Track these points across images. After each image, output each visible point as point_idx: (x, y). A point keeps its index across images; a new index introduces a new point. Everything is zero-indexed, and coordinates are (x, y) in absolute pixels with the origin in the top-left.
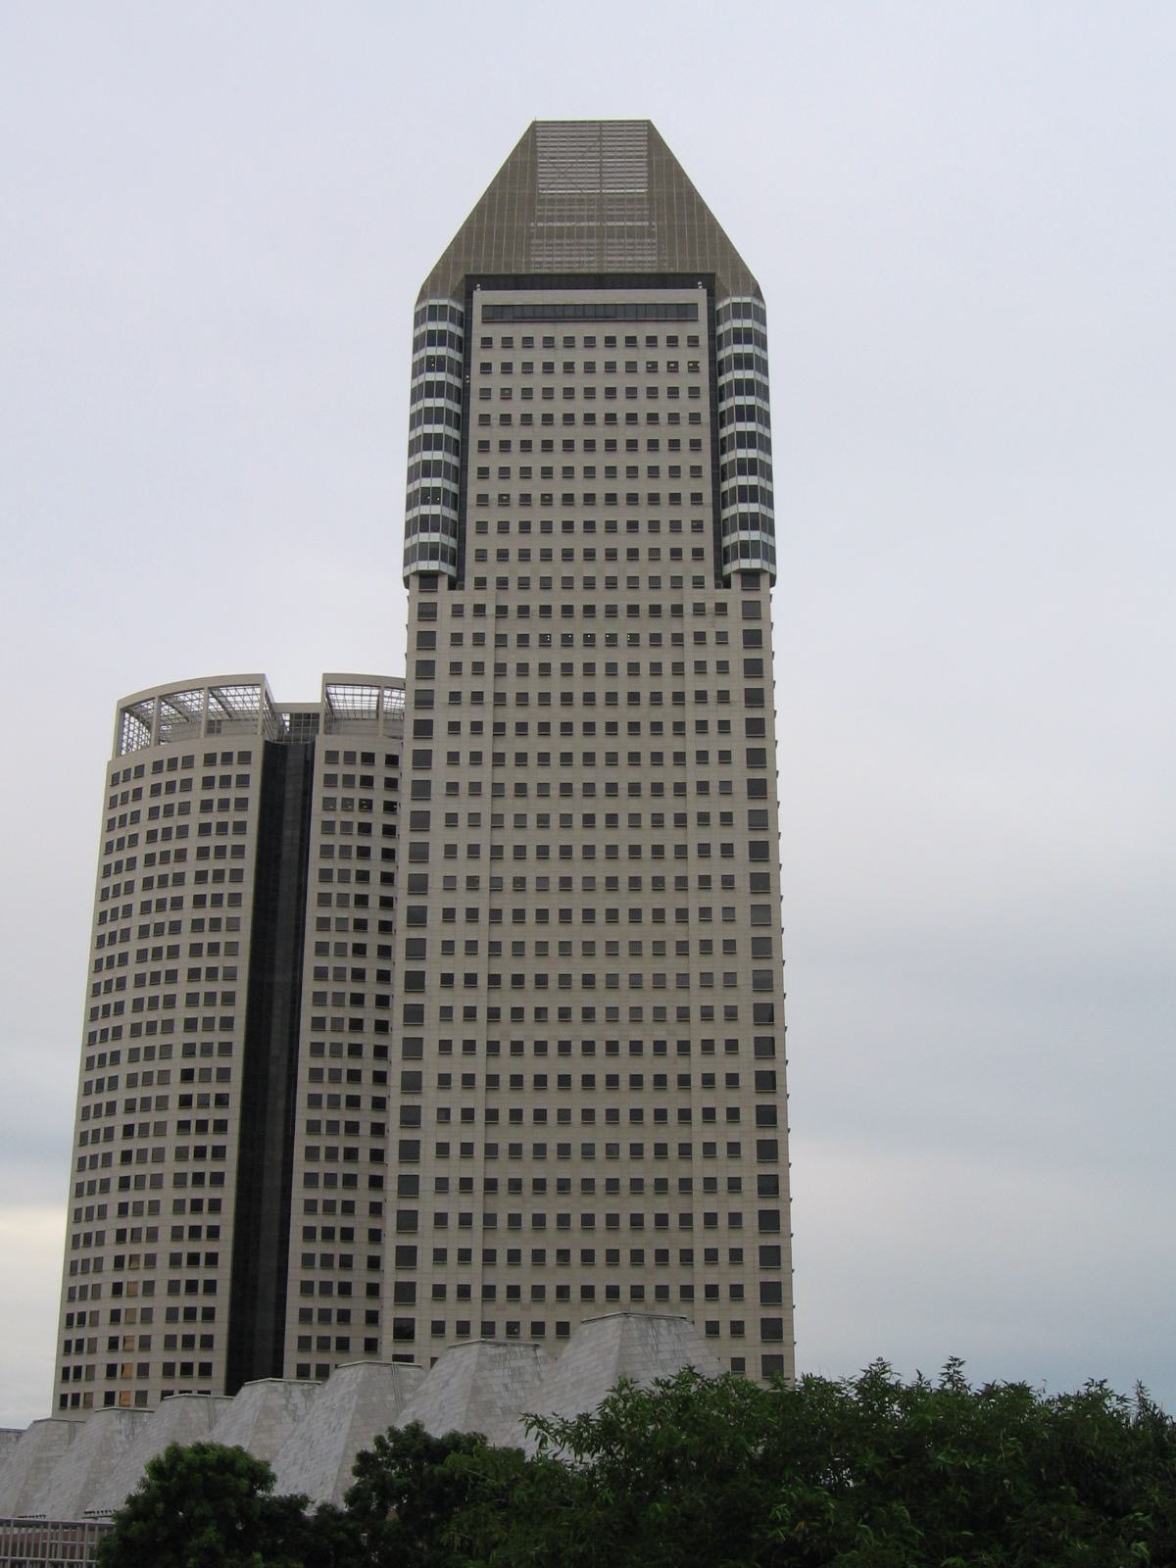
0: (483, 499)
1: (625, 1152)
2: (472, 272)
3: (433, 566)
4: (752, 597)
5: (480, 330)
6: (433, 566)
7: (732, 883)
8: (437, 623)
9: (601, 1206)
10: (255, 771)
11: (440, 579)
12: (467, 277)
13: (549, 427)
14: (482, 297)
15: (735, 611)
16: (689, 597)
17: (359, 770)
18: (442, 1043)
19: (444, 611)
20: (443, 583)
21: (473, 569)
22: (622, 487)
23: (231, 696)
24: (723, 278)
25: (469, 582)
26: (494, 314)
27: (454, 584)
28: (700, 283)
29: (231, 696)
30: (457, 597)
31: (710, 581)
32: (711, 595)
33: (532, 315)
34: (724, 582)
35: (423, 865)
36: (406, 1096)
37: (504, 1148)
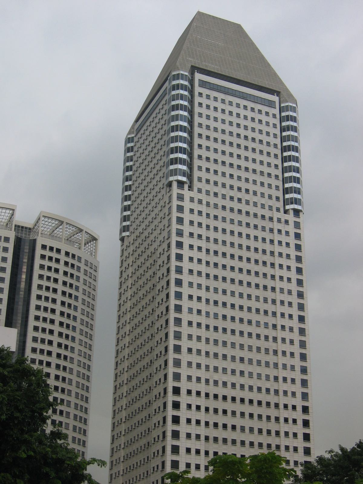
2: (193, 65)
3: (184, 179)
4: (297, 220)
5: (198, 89)
6: (184, 179)
7: (294, 368)
8: (184, 214)
10: (11, 246)
11: (185, 185)
12: (192, 66)
14: (198, 76)
16: (276, 215)
17: (54, 255)
18: (188, 376)
19: (187, 198)
20: (186, 187)
21: (197, 185)
22: (259, 168)
25: (195, 189)
26: (203, 84)
27: (190, 188)
28: (275, 94)
30: (191, 194)
31: (282, 210)
32: (284, 217)
33: (235, 94)
34: (286, 212)
35: (181, 238)
36: (176, 340)
37: (211, 424)
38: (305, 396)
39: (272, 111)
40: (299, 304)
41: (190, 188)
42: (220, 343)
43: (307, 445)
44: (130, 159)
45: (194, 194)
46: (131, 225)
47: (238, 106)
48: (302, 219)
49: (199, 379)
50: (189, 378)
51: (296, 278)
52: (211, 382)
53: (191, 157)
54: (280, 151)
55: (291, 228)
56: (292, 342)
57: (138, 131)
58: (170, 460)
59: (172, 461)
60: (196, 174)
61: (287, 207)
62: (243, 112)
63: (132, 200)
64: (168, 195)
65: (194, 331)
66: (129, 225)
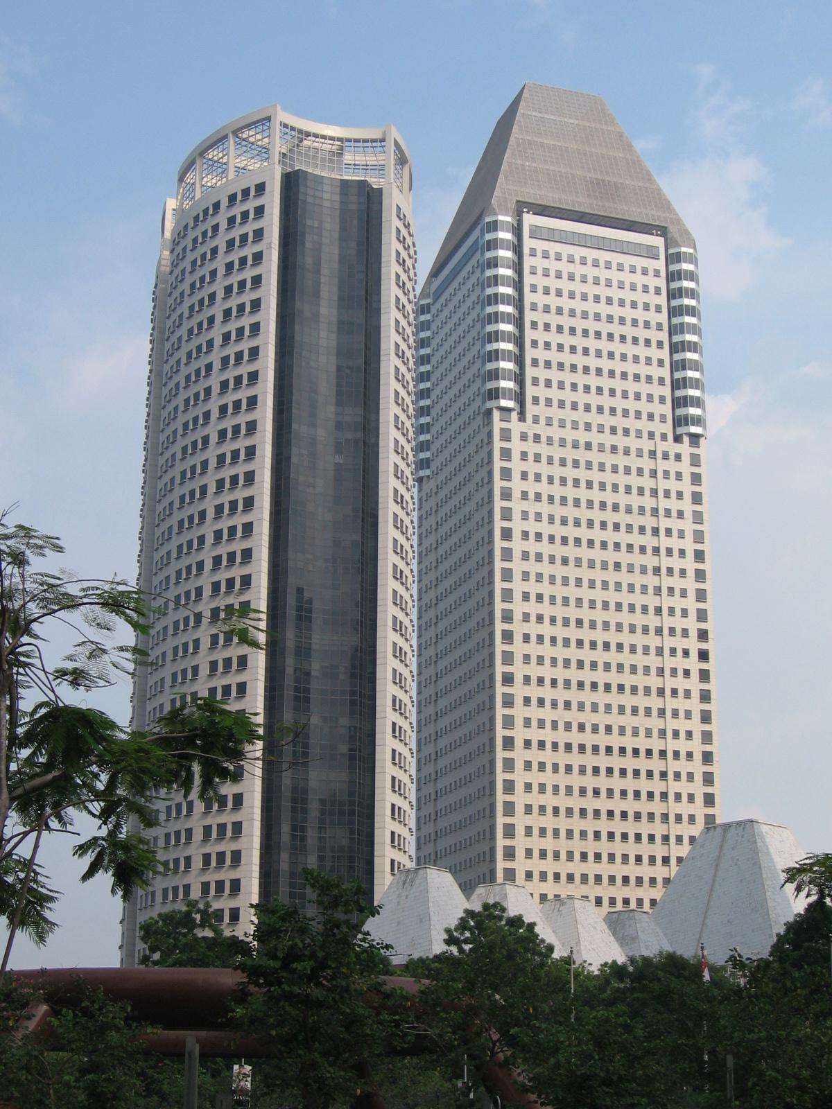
0: (535, 362)
1: (588, 728)
5: (528, 243)
7: (682, 496)
9: (618, 826)
13: (605, 551)
14: (529, 220)
15: (686, 458)
21: (531, 410)
23: (259, 140)
24: (673, 230)
26: (536, 233)
27: (522, 417)
29: (259, 140)
30: (523, 427)
31: (670, 437)
32: (673, 448)
34: (678, 439)
38: (702, 616)
39: (652, 264)
40: (699, 610)
41: (522, 417)
42: (596, 486)
43: (704, 666)
44: (423, 394)
45: (529, 427)
46: (433, 321)
47: (596, 264)
48: (703, 449)
49: (540, 598)
50: (525, 535)
51: (698, 669)
52: (561, 726)
53: (520, 324)
54: (665, 281)
55: (686, 468)
56: (680, 514)
57: (437, 296)
58: (502, 868)
59: (504, 781)
60: (530, 391)
61: (679, 431)
62: (590, 271)
63: (432, 346)
64: (487, 429)
65: (531, 467)
66: (428, 441)
